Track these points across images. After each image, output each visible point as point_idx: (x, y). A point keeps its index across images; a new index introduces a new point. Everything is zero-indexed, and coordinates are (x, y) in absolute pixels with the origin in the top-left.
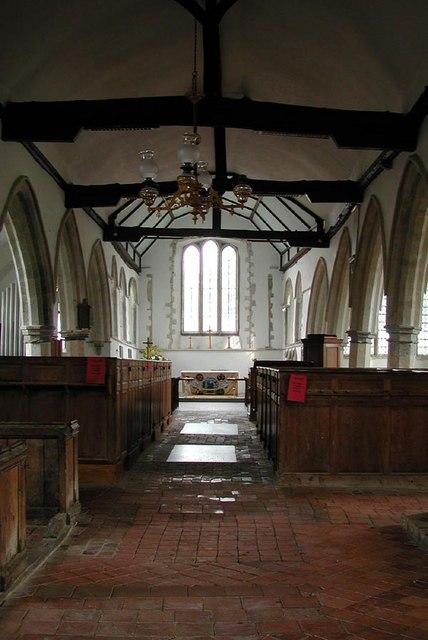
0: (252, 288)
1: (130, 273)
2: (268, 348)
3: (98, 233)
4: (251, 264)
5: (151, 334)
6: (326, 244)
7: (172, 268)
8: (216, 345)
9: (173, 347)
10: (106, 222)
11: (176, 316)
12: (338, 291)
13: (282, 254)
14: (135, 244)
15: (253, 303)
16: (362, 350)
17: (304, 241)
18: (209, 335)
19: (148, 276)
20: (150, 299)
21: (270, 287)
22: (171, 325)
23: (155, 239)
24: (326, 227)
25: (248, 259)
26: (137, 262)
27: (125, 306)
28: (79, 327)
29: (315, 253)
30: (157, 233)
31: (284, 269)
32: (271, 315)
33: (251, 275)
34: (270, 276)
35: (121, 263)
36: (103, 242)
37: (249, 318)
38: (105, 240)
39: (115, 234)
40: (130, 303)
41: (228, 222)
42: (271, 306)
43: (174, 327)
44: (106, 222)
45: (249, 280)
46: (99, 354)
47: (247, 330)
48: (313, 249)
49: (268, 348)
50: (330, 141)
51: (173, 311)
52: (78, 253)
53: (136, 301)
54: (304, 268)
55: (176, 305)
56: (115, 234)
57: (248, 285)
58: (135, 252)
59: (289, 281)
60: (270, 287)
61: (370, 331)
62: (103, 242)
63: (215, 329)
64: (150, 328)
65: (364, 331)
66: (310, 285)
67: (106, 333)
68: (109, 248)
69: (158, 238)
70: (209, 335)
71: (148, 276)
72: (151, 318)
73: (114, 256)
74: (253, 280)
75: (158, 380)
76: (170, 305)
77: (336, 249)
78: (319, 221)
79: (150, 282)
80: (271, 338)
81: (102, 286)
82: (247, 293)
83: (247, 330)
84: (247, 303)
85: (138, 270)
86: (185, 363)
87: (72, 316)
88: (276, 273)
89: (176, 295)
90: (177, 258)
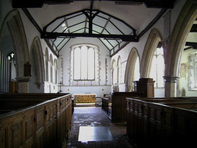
0: (100, 63)
1: (54, 57)
2: (106, 85)
3: (38, 34)
4: (99, 55)
5: (63, 80)
6: (137, 41)
7: (70, 56)
8: (87, 84)
9: (71, 85)
10: (42, 29)
11: (72, 74)
12: (146, 60)
13: (110, 51)
14: (53, 40)
15: (100, 69)
16: (173, 86)
17: (127, 39)
18: (84, 80)
19: (62, 59)
20: (62, 67)
21: (106, 63)
22: (70, 77)
23: (65, 38)
24: (138, 33)
25: (98, 53)
26: (57, 53)
27: (51, 68)
28: (25, 75)
29: (131, 45)
30: (63, 35)
31: (111, 56)
32: (106, 73)
33: (99, 58)
34: (106, 59)
35: (50, 52)
36: (41, 39)
37: (99, 74)
38: (42, 38)
39: (46, 35)
40: (54, 68)
41: (96, 30)
42: (106, 69)
43: (71, 77)
44: (42, 29)
45: (98, 60)
46: (128, 91)
47: (98, 78)
48: (131, 42)
49: (106, 85)
50: (143, 6)
51: (70, 71)
52: (22, 28)
53: (57, 68)
54: (124, 54)
55: (72, 69)
56: (46, 35)
57: (98, 62)
58: (56, 49)
59: (114, 60)
60: (106, 63)
61: (177, 76)
62: (41, 39)
63: (86, 79)
64: (62, 78)
65: (174, 76)
66: (127, 59)
67: (42, 79)
68: (43, 41)
69: (66, 37)
70: (84, 80)
71: (62, 59)
72: (62, 74)
73: (47, 48)
74: (100, 60)
75: (64, 110)
76: (69, 69)
77: (146, 40)
78: (134, 31)
79: (62, 61)
80: (107, 81)
81: (41, 59)
82: (98, 65)
83: (98, 78)
84: (98, 69)
85: (58, 56)
86: (75, 91)
87: (22, 70)
88: (108, 58)
89: (72, 65)
90: (72, 52)
